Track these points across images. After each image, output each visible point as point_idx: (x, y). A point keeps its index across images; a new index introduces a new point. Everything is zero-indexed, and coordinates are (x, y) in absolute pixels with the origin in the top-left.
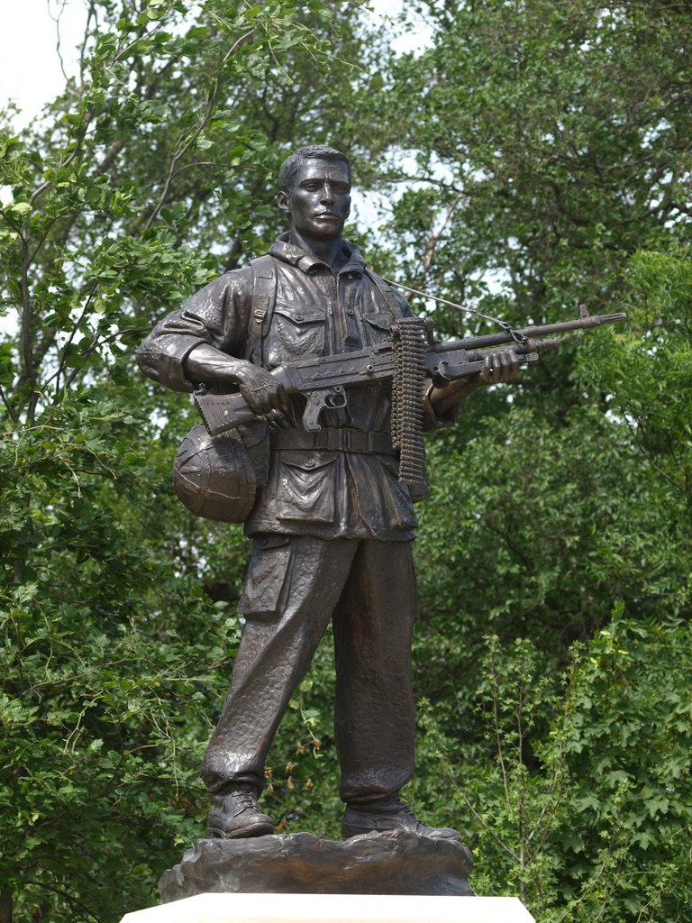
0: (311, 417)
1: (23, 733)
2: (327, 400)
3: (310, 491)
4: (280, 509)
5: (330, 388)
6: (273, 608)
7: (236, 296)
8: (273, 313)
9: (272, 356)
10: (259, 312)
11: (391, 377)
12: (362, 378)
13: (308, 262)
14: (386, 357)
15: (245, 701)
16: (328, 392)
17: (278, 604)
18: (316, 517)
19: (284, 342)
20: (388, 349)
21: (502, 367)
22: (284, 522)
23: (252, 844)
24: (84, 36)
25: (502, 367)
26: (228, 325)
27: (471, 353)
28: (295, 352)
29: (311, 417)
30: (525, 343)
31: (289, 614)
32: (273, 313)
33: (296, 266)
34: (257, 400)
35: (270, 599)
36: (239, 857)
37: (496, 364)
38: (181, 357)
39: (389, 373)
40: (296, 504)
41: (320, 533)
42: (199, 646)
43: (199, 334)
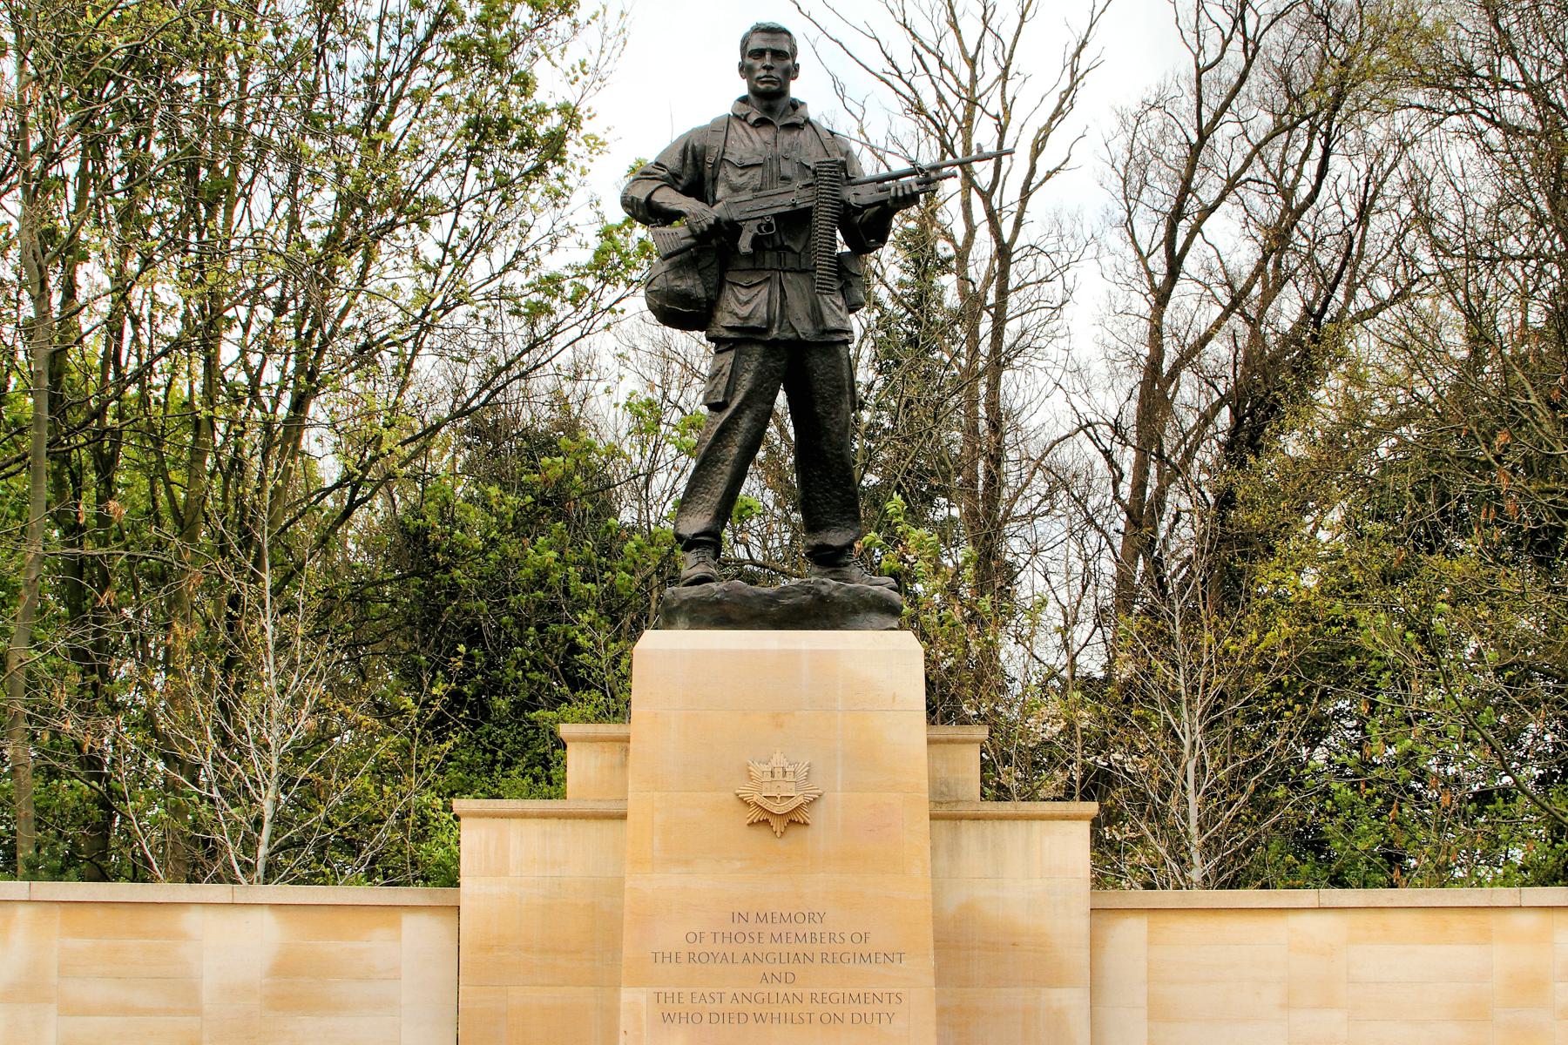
0: (745, 244)
1: (476, 552)
2: (759, 227)
3: (747, 303)
4: (724, 319)
5: (762, 218)
6: (720, 400)
7: (694, 147)
8: (722, 159)
9: (719, 195)
10: (710, 159)
11: (811, 208)
12: (788, 209)
13: (753, 118)
14: (809, 192)
15: (702, 476)
16: (759, 221)
17: (726, 394)
18: (752, 323)
19: (728, 182)
20: (811, 185)
21: (905, 195)
22: (729, 329)
23: (694, 591)
24: (1019, 19)
25: (905, 195)
26: (689, 170)
27: (880, 186)
28: (736, 190)
29: (745, 244)
30: (927, 175)
31: (734, 404)
32: (722, 159)
33: (745, 120)
34: (698, 230)
35: (719, 392)
36: (686, 601)
37: (1495, 200)
38: (643, 199)
39: (809, 205)
40: (736, 314)
41: (759, 337)
42: (266, 528)
43: (663, 179)
